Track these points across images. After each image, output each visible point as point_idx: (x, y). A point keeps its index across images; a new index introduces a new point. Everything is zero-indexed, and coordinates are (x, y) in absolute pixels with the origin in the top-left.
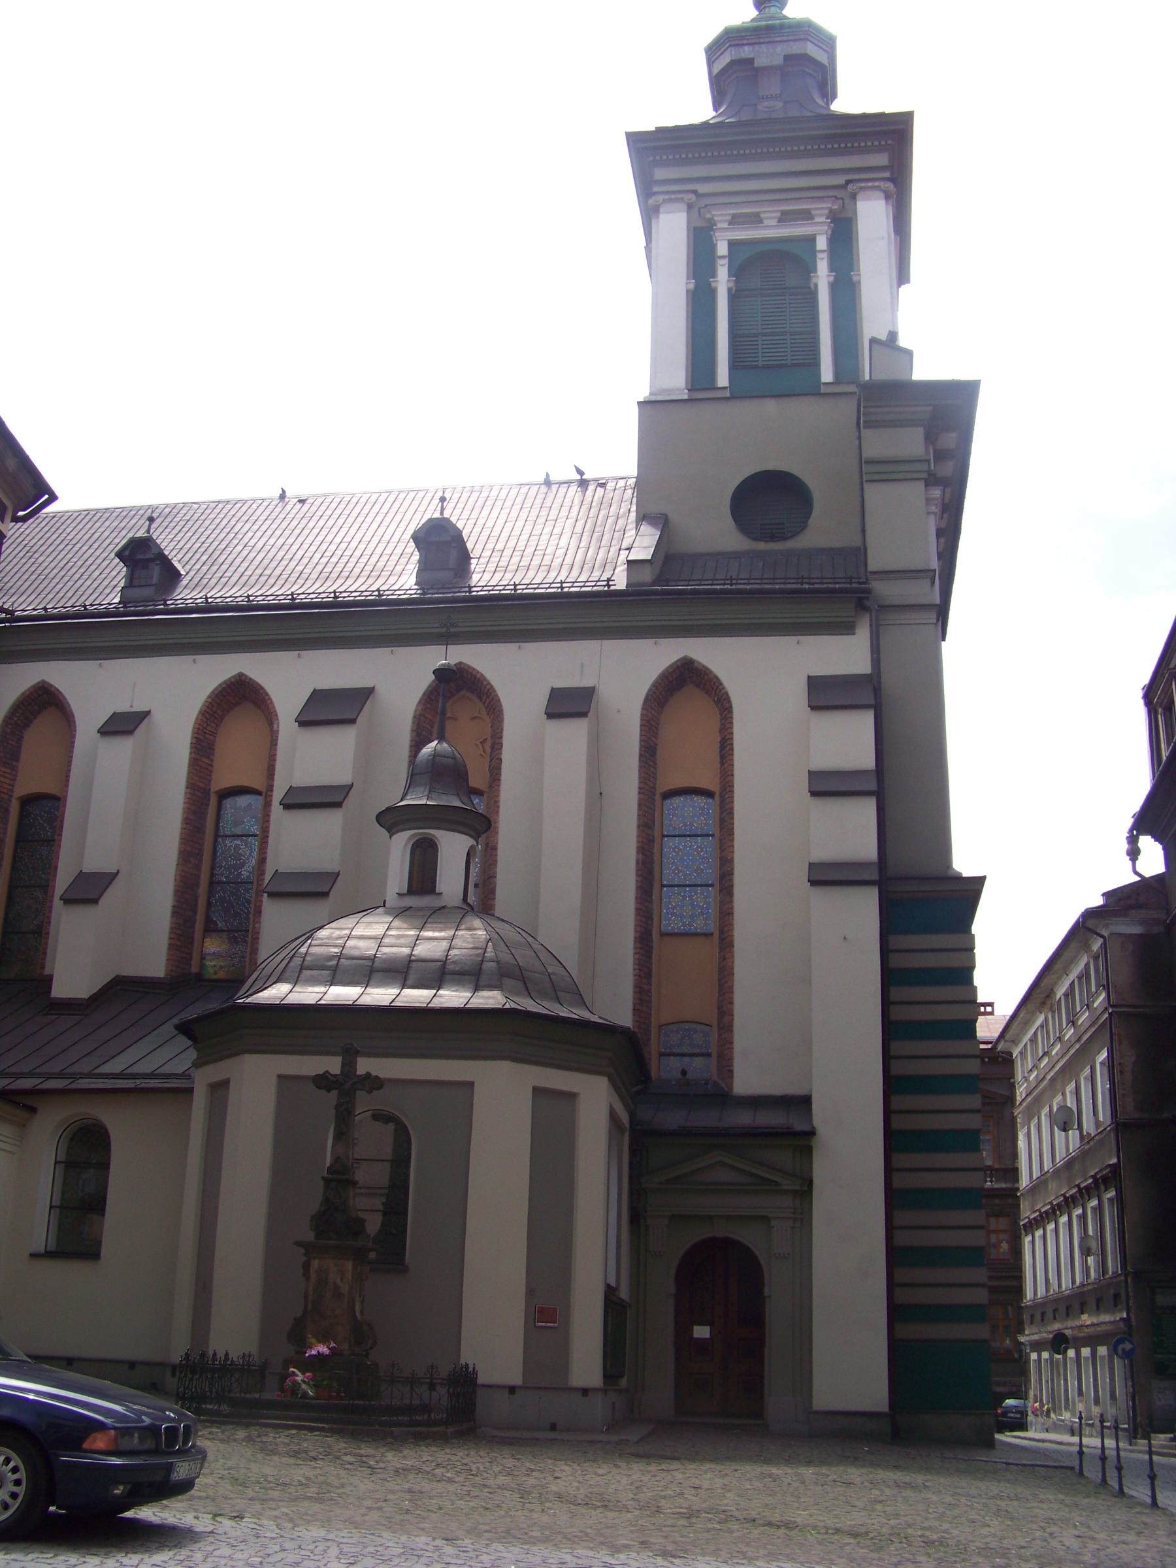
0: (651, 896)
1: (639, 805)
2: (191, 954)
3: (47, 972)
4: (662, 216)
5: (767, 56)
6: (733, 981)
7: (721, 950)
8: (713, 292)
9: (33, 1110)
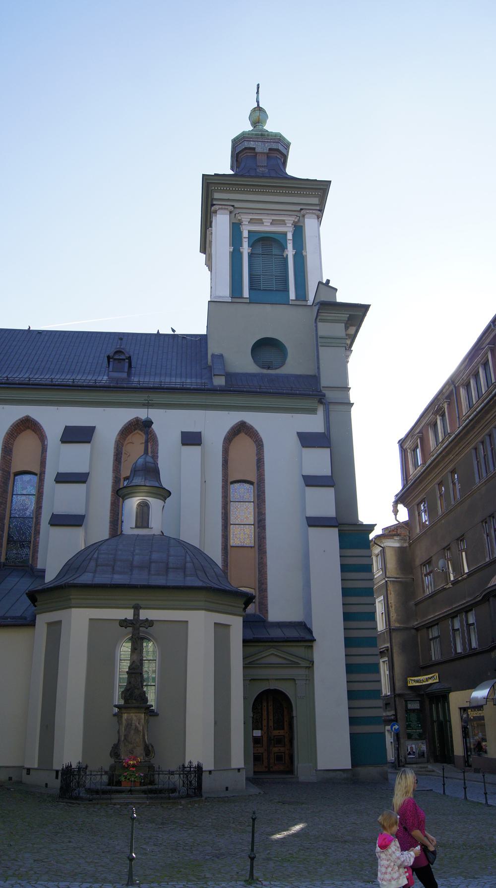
1: (222, 487)
6: (267, 569)
7: (259, 554)
8: (241, 254)
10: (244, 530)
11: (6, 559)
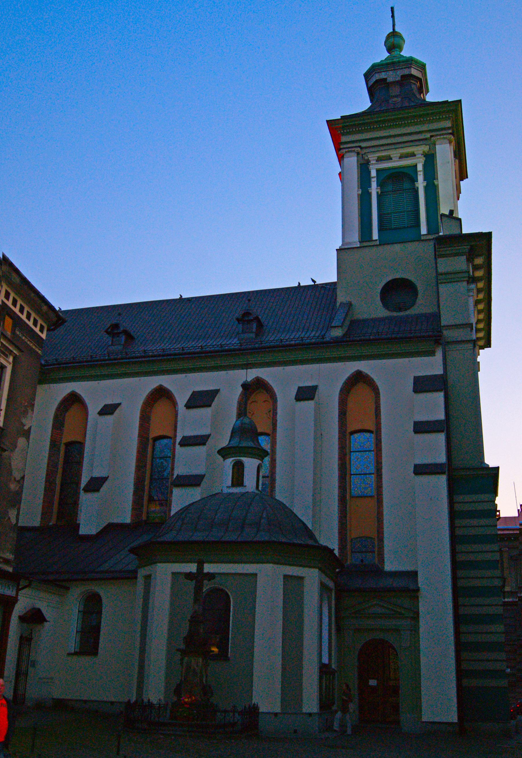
0: (346, 479)
2: (142, 511)
3: (78, 522)
4: (345, 159)
5: (392, 76)
8: (370, 194)
9: (68, 589)
10: (364, 480)
11: (148, 517)
